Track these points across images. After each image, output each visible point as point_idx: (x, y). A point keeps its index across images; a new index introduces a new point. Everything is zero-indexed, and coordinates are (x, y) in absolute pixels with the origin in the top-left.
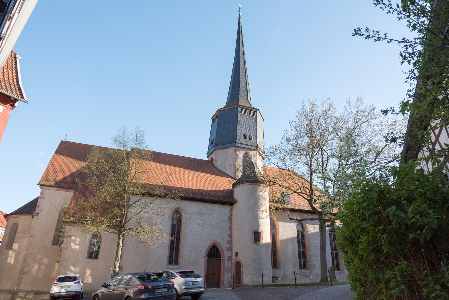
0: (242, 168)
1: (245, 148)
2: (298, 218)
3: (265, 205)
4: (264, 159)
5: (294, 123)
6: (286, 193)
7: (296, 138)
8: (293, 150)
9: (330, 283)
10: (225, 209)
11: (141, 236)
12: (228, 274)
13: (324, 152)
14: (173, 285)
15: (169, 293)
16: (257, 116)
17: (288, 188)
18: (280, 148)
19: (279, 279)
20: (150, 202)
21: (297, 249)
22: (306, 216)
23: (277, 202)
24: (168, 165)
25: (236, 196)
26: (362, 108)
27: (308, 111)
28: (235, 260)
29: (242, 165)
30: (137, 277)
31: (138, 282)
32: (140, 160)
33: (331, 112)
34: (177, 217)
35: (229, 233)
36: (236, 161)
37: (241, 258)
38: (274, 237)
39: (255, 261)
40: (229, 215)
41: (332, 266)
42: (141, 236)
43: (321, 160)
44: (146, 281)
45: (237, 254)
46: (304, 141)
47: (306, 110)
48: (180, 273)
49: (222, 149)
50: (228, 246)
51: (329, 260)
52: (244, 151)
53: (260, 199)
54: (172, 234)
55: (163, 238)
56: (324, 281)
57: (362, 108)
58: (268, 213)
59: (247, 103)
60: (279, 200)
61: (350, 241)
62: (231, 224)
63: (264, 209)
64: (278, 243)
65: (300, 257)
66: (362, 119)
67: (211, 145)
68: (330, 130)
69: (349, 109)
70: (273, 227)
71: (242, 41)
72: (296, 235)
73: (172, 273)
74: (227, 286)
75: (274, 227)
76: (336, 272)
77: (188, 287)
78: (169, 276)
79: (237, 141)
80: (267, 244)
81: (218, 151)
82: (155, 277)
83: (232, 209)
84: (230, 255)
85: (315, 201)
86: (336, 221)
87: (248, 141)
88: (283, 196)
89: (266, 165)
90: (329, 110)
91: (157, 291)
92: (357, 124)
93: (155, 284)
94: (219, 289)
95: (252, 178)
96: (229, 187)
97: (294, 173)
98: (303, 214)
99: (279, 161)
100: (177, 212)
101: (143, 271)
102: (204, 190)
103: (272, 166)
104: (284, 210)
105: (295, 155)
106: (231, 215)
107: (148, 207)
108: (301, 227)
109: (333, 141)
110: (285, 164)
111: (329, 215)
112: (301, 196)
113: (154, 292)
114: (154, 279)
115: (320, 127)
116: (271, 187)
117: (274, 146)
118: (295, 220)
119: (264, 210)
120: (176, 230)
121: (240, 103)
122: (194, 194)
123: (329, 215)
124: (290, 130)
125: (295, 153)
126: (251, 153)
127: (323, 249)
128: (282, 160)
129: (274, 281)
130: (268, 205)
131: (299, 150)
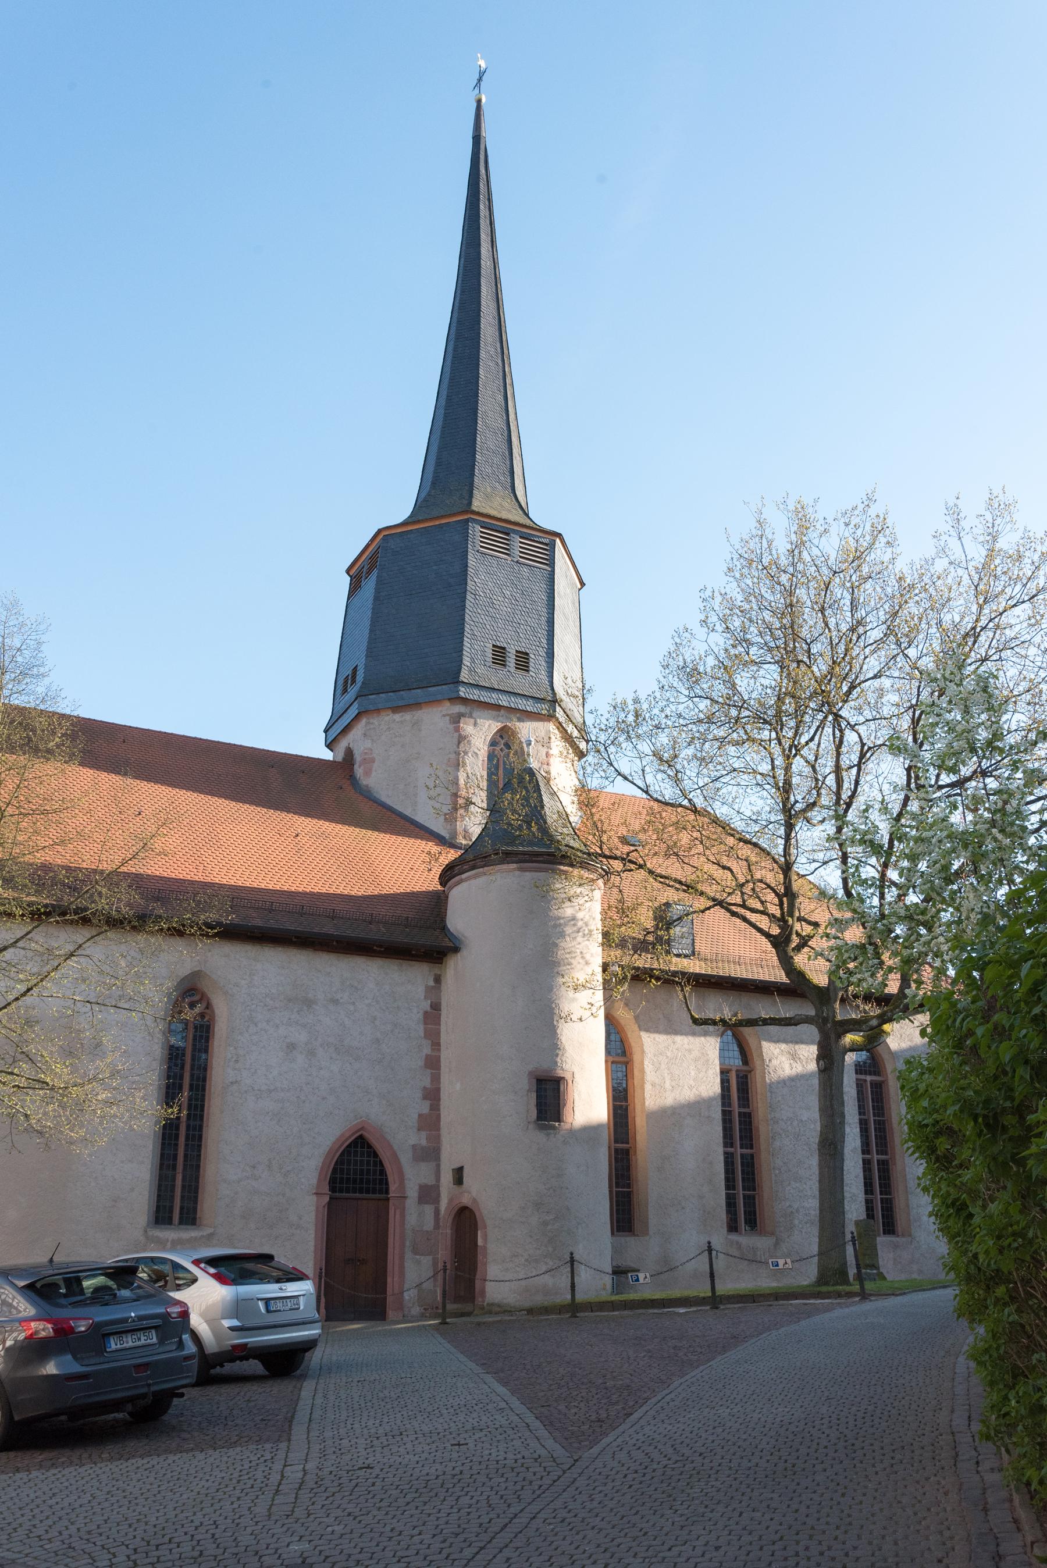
0: (484, 795)
1: (498, 707)
2: (727, 1014)
3: (586, 959)
4: (581, 755)
5: (718, 599)
6: (677, 910)
7: (727, 669)
8: (710, 720)
9: (856, 1288)
10: (408, 981)
11: (32, 1103)
12: (419, 1262)
13: (847, 732)
14: (185, 1314)
15: (168, 1352)
16: (551, 563)
17: (688, 887)
18: (656, 711)
19: (641, 1276)
20: (71, 948)
21: (720, 1150)
22: (763, 1008)
23: (641, 946)
24: (148, 780)
25: (457, 920)
26: (1007, 542)
27: (782, 546)
28: (451, 1200)
29: (484, 784)
30: (22, 1283)
31: (25, 1307)
32: (22, 759)
33: (880, 554)
34: (189, 1015)
35: (427, 1082)
36: (457, 765)
37: (478, 1190)
38: (621, 1098)
39: (538, 1206)
40: (426, 1005)
41: (863, 1216)
42: (32, 1103)
43: (831, 764)
44: (63, 1301)
45: (459, 1176)
46: (760, 682)
47: (770, 543)
48: (212, 1262)
49: (396, 709)
50: (422, 1139)
51: (854, 1190)
52: (495, 719)
53: (562, 935)
54: (170, 1094)
55: (128, 1111)
56: (832, 1280)
57: (1007, 542)
58: (599, 995)
59: (508, 503)
60: (650, 938)
61: (985, 1117)
62: (436, 1045)
63: (580, 975)
64: (640, 1124)
65: (730, 1182)
66: (1008, 590)
67: (345, 691)
68: (875, 634)
69: (954, 543)
70: (620, 1054)
71: (492, 223)
72: (717, 1089)
73: (176, 1266)
74: (416, 1310)
75: (624, 1053)
76: (882, 1240)
77: (248, 1324)
78: (159, 1277)
79: (464, 675)
80: (590, 1131)
81: (375, 721)
82: (100, 1280)
83: (438, 980)
84: (430, 1181)
85: (804, 942)
86: (886, 1027)
87: (511, 678)
88: (664, 919)
89: (593, 783)
90: (871, 546)
91: (114, 1344)
92: (986, 611)
93: (103, 1314)
94: (380, 1327)
95: (531, 843)
96: (428, 881)
97: (715, 821)
98: (746, 998)
99: (651, 766)
100: (191, 992)
101: (45, 1260)
102: (282, 893)
103: (621, 787)
104: (670, 980)
105: (722, 741)
106: (436, 1007)
107: (62, 970)
108: (737, 1054)
109: (886, 682)
110: (677, 780)
111: (859, 1002)
112: (745, 919)
113: (100, 1349)
114: (97, 1290)
115: (832, 622)
116: (615, 879)
117: (630, 702)
118: (714, 1023)
119: (582, 981)
120: (187, 1071)
121: (476, 505)
122: (271, 911)
123: (859, 1002)
124: (701, 632)
125: (721, 733)
126: (527, 730)
127: (830, 1146)
128: (666, 761)
129: (617, 1288)
130: (599, 961)
131: (737, 719)
